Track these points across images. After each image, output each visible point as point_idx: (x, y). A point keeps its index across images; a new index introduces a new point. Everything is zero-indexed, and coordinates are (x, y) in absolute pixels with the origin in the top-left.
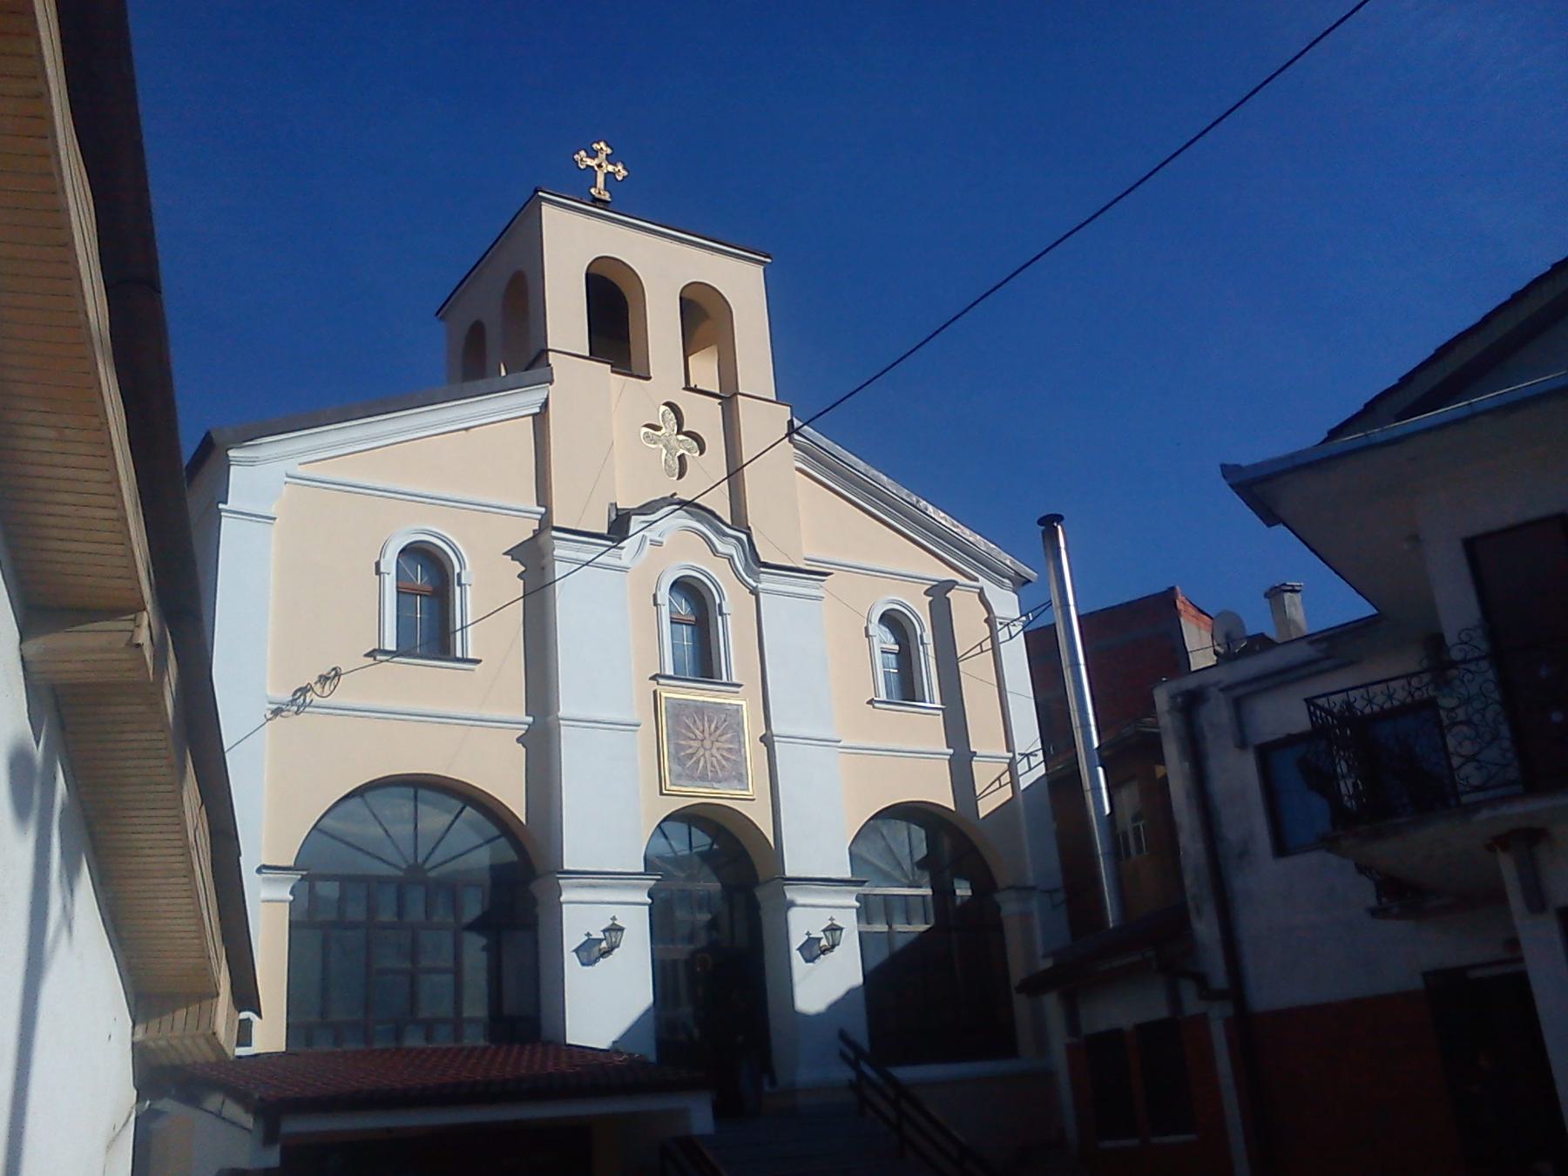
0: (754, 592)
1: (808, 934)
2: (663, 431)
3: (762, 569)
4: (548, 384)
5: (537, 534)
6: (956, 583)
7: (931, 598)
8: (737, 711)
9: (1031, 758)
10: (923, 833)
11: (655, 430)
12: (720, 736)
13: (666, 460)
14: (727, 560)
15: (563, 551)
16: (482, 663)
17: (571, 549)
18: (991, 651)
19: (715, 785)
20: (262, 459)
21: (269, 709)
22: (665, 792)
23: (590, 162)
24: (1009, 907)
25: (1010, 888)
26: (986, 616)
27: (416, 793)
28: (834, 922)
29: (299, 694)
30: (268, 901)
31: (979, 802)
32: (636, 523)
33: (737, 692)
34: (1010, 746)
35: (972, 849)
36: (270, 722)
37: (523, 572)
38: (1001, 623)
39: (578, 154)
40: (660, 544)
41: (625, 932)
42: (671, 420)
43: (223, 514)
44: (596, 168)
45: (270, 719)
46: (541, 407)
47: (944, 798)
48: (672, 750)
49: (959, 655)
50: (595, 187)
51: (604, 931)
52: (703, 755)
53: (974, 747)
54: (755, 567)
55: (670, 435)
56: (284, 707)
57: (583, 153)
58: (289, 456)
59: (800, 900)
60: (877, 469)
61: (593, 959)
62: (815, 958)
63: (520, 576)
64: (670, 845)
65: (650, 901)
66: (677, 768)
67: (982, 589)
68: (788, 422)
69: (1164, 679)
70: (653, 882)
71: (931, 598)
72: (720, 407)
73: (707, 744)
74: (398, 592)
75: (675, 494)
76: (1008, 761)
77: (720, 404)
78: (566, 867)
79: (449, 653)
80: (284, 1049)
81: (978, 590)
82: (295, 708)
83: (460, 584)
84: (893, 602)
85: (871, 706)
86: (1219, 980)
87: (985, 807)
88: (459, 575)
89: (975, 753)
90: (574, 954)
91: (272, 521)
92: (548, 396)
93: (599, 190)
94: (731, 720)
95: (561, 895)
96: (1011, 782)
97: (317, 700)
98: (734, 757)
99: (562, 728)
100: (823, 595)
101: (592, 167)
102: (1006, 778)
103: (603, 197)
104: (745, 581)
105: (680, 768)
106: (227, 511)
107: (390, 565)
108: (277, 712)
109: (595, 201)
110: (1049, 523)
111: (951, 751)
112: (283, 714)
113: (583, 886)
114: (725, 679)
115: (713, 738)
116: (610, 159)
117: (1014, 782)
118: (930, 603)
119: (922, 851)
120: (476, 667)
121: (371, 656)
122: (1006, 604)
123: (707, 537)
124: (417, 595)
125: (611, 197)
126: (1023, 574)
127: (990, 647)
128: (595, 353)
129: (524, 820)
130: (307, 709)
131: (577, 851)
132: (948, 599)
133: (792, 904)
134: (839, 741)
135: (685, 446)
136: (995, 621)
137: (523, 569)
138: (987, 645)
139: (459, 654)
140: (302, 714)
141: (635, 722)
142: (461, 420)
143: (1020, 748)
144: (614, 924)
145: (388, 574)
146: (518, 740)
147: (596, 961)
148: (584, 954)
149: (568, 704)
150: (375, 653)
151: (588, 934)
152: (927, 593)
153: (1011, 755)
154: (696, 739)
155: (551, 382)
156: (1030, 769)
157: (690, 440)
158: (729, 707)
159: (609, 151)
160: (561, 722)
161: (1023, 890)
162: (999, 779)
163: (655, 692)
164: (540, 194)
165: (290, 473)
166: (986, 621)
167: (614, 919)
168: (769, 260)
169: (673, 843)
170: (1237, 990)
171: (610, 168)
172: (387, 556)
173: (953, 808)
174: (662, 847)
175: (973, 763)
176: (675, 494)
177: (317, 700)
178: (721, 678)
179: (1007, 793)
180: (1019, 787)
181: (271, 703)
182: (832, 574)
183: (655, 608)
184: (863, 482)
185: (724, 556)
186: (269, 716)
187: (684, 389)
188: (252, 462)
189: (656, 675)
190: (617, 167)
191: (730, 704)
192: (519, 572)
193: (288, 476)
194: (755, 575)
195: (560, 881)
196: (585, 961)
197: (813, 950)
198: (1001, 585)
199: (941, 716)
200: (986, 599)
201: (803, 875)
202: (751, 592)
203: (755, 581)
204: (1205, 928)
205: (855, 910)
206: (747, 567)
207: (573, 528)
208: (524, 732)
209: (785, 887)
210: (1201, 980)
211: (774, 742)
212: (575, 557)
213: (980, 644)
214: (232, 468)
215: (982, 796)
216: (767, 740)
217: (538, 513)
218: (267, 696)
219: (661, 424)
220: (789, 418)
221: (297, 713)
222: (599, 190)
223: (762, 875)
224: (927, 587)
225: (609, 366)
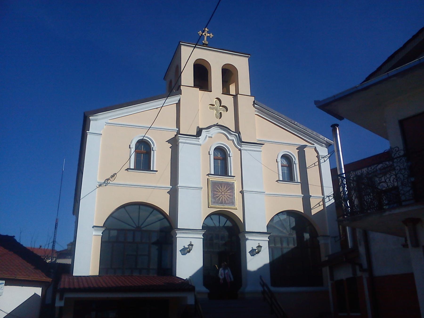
0: (240, 150)
1: (252, 248)
2: (215, 106)
3: (242, 143)
4: (180, 95)
5: (176, 135)
6: (307, 146)
7: (298, 150)
8: (233, 184)
9: (330, 197)
10: (294, 220)
11: (213, 106)
12: (227, 191)
13: (216, 114)
14: (232, 141)
15: (181, 140)
16: (235, 177)
17: (184, 140)
18: (318, 166)
19: (225, 205)
20: (99, 119)
21: (98, 185)
22: (209, 207)
24: (322, 241)
25: (321, 236)
26: (317, 155)
27: (139, 207)
28: (260, 245)
29: (106, 180)
30: (96, 235)
31: (312, 210)
32: (204, 132)
33: (233, 179)
34: (323, 194)
35: (310, 224)
36: (98, 188)
37: (171, 146)
38: (321, 157)
39: (199, 32)
40: (211, 137)
41: (262, 247)
42: (218, 103)
43: (88, 134)
44: (204, 35)
45: (98, 187)
46: (178, 101)
47: (300, 209)
48: (212, 195)
49: (307, 167)
50: (204, 40)
51: (257, 247)
52: (222, 196)
53: (311, 194)
54: (241, 143)
55: (218, 107)
56: (102, 184)
58: (106, 118)
59: (250, 238)
60: (281, 113)
61: (185, 253)
62: (254, 255)
63: (170, 148)
64: (213, 222)
66: (213, 200)
67: (315, 147)
68: (253, 101)
69: (352, 172)
70: (204, 232)
71: (298, 150)
72: (233, 98)
73: (223, 193)
74: (214, 159)
75: (218, 123)
76: (322, 198)
77: (233, 97)
79: (227, 175)
80: (98, 274)
81: (314, 148)
82: (105, 184)
84: (288, 152)
85: (277, 182)
86: (365, 265)
87: (314, 212)
89: (311, 196)
91: (101, 135)
92: (180, 98)
93: (205, 41)
94: (230, 186)
95: (177, 235)
96: (323, 204)
97: (111, 182)
98: (231, 197)
99: (179, 189)
100: (262, 150)
102: (322, 203)
103: (206, 43)
104: (238, 147)
105: (214, 200)
106: (89, 133)
107: (212, 152)
108: (100, 185)
109: (204, 44)
110: (334, 127)
111: (303, 195)
112: (102, 186)
113: (183, 233)
114: (152, 169)
116: (208, 32)
117: (324, 204)
118: (298, 152)
119: (293, 224)
120: (234, 178)
121: (208, 175)
122: (324, 151)
123: (226, 134)
124: (219, 160)
125: (208, 43)
126: (329, 142)
127: (318, 164)
128: (195, 86)
129: (168, 215)
130: (108, 184)
132: (304, 151)
133: (247, 239)
134: (265, 193)
135: (222, 110)
136: (320, 157)
137: (171, 145)
138: (317, 163)
139: (230, 175)
140: (107, 186)
141: (263, 191)
143: (326, 194)
144: (191, 243)
145: (133, 148)
146: (168, 193)
147: (186, 254)
148: (183, 252)
149: (181, 183)
150: (128, 169)
151: (184, 246)
152: (297, 149)
153: (323, 196)
154: (220, 192)
155: (181, 95)
156: (329, 200)
157: (223, 108)
158: (230, 183)
159: (208, 30)
160: (179, 187)
161: (324, 236)
162: (319, 203)
163: (208, 179)
164: (181, 43)
166: (317, 157)
168: (250, 56)
169: (214, 221)
170: (370, 269)
171: (208, 35)
172: (211, 150)
173: (303, 212)
174: (211, 223)
175: (310, 199)
176: (218, 123)
177: (111, 182)
178: (295, 181)
179: (321, 208)
180: (325, 206)
181: (98, 183)
182: (264, 144)
184: (276, 117)
186: (98, 186)
187: (222, 94)
188: (96, 120)
189: (209, 174)
190: (210, 34)
191: (230, 182)
192: (170, 146)
193: (106, 123)
194: (241, 146)
195: (176, 231)
197: (254, 252)
198: (322, 146)
199: (300, 185)
200: (317, 150)
201: (251, 231)
202: (239, 150)
203: (240, 147)
204: (362, 250)
205: (268, 241)
206: (238, 143)
207: (186, 134)
208: (169, 190)
209: (245, 234)
210: (361, 266)
211: (244, 193)
212: (185, 142)
213: (314, 164)
214: (91, 122)
215: (313, 209)
216: (242, 192)
217: (176, 130)
218: (97, 181)
219: (215, 104)
220: (254, 100)
222: (205, 41)
223: (241, 230)
224: (297, 147)
225: (199, 89)
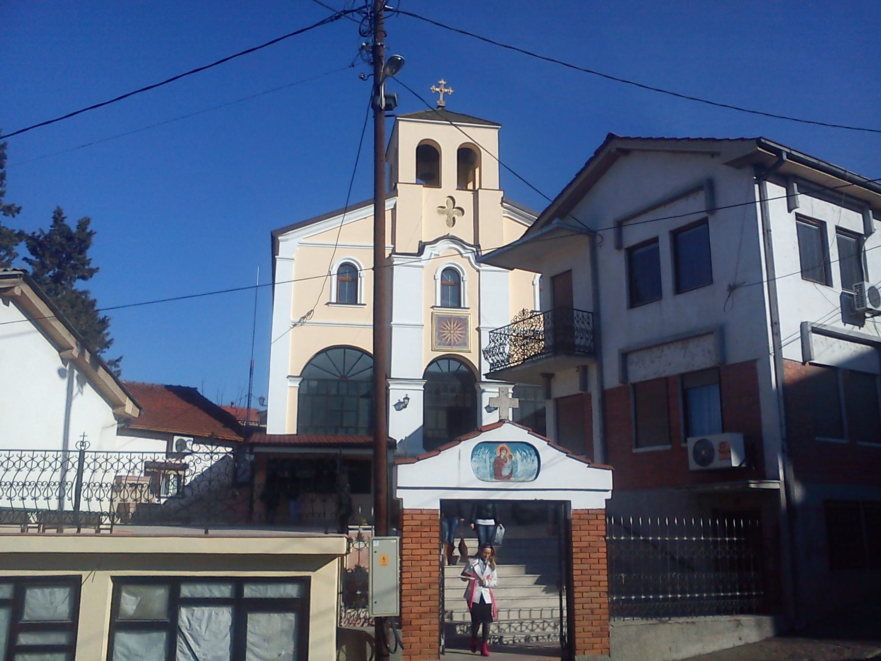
0: (478, 271)
8: (466, 319)
23: (437, 90)
57: (434, 86)
59: (487, 390)
65: (423, 389)
66: (439, 341)
72: (472, 195)
73: (452, 332)
78: (392, 377)
82: (300, 324)
83: (463, 281)
88: (463, 277)
90: (394, 407)
97: (307, 321)
101: (438, 92)
107: (335, 271)
108: (294, 325)
115: (455, 329)
116: (446, 87)
131: (396, 371)
133: (484, 391)
142: (362, 215)
148: (397, 407)
151: (399, 400)
165: (301, 242)
167: (407, 395)
168: (500, 127)
171: (446, 90)
183: (434, 281)
185: (465, 257)
186: (292, 326)
188: (287, 240)
193: (299, 243)
196: (398, 409)
202: (477, 271)
207: (403, 252)
221: (301, 325)
